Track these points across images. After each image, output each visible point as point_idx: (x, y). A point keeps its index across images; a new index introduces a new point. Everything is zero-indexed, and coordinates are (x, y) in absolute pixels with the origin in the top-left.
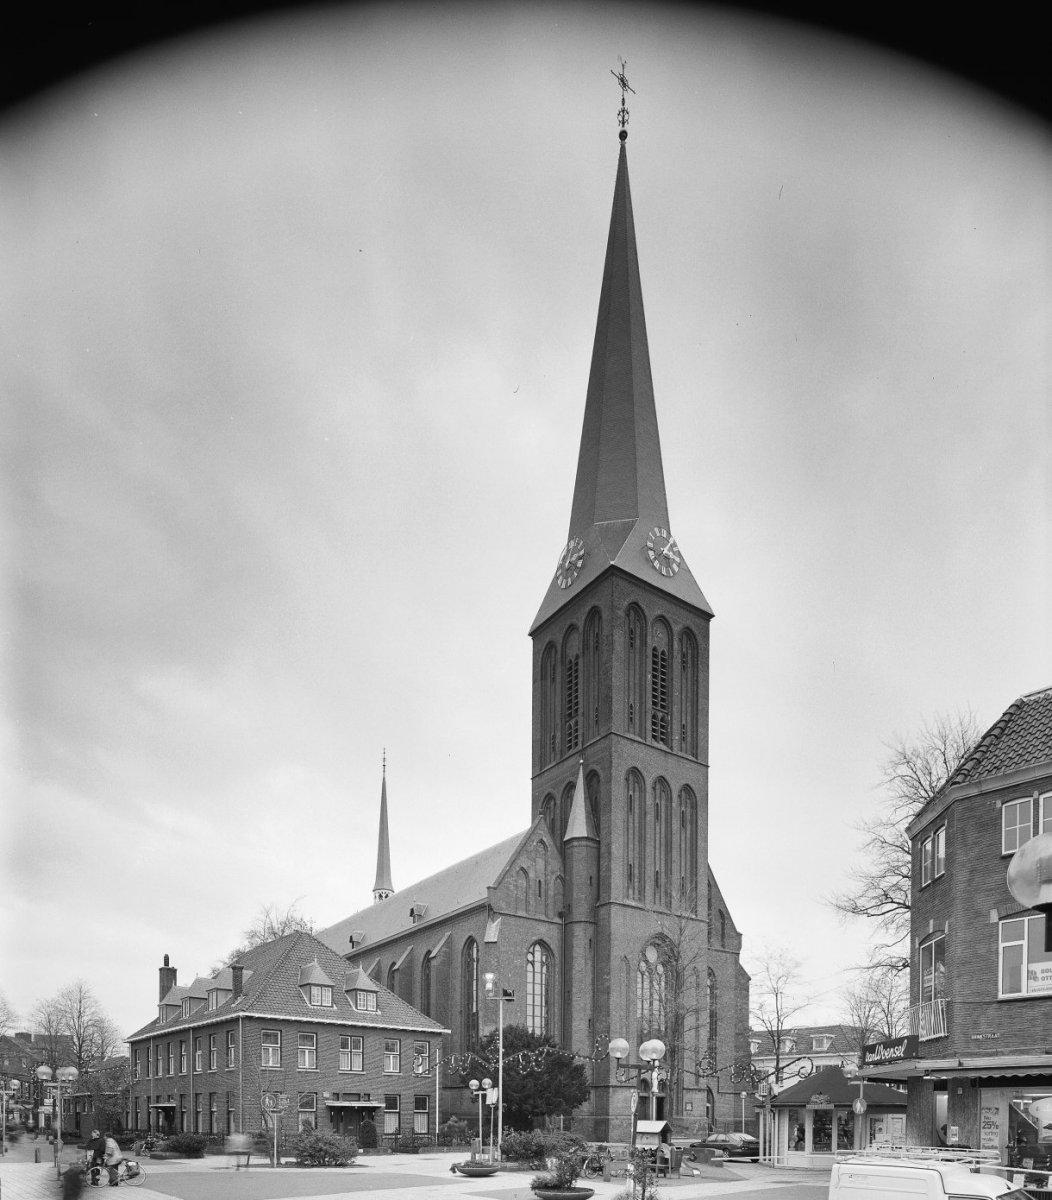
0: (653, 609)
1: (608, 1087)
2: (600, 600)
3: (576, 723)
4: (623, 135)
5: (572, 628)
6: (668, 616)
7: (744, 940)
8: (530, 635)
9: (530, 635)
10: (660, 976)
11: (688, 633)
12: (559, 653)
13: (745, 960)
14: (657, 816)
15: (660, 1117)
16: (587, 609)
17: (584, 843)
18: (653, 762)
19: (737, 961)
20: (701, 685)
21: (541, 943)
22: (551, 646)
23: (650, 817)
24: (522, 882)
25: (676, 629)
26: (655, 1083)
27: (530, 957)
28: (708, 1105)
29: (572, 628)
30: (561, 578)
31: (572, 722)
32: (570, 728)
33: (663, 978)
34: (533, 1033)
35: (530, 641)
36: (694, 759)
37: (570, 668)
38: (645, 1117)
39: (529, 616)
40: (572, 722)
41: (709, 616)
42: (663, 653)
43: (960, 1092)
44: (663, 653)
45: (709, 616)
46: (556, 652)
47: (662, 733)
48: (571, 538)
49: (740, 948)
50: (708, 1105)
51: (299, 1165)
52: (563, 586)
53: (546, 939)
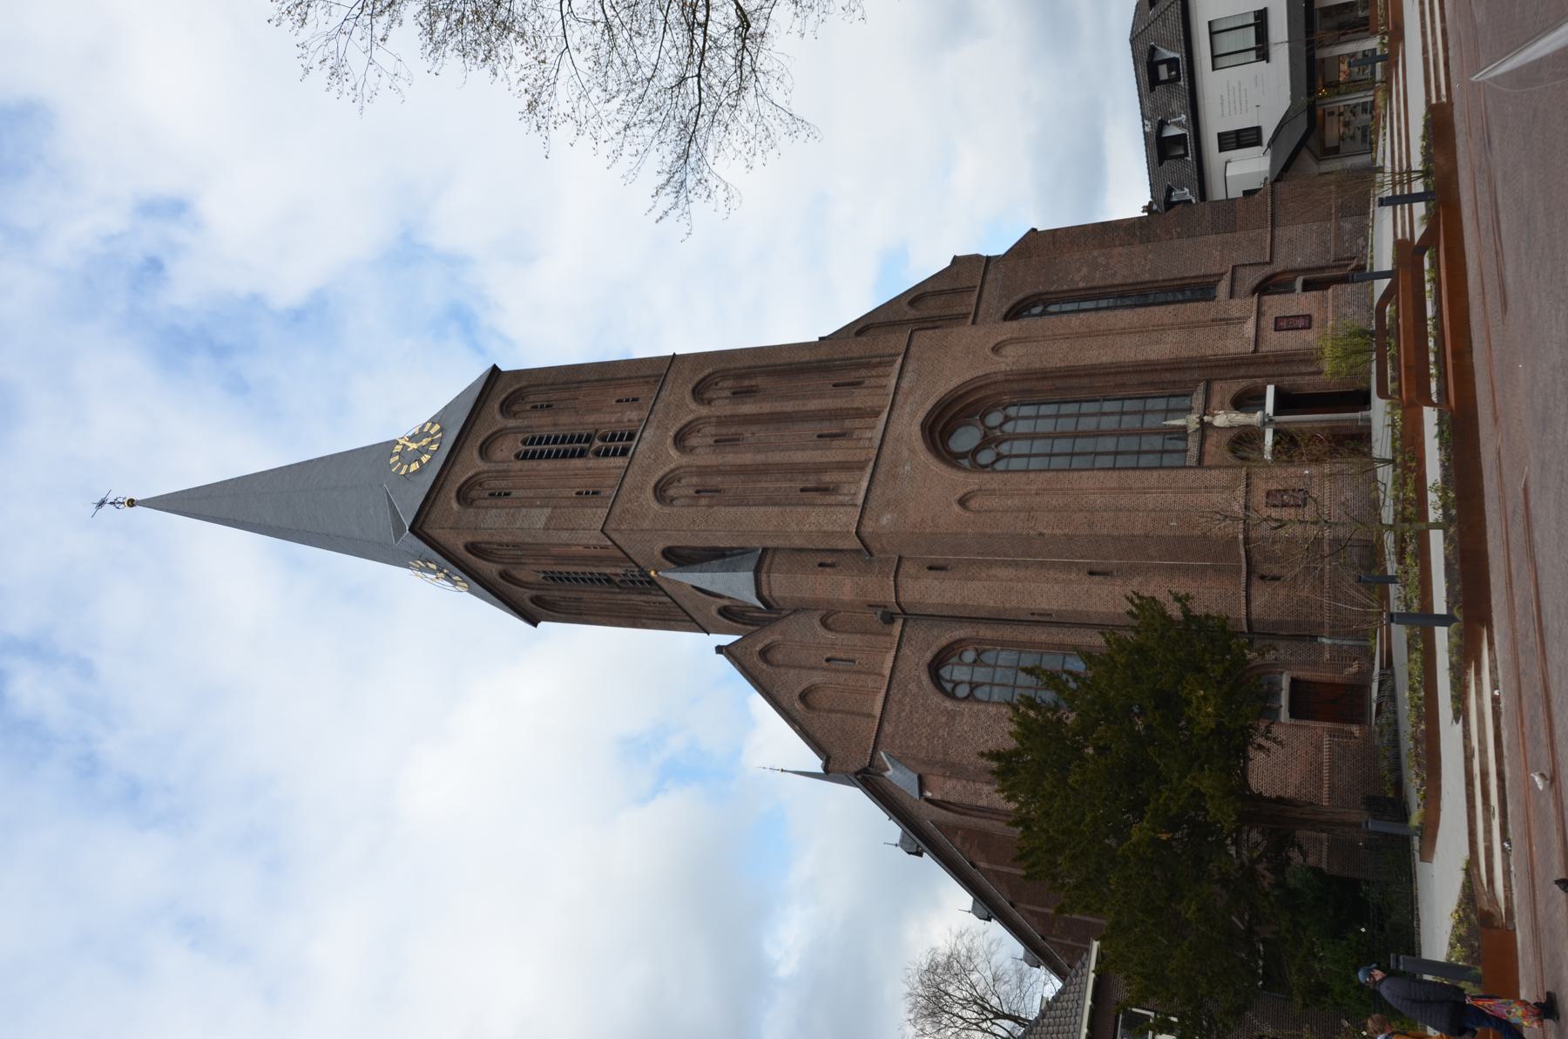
2: (457, 543)
4: (131, 503)
5: (505, 575)
7: (963, 252)
10: (1007, 419)
11: (506, 408)
15: (1362, 401)
17: (764, 577)
21: (935, 668)
25: (501, 422)
26: (1240, 418)
27: (962, 691)
28: (1299, 284)
32: (622, 581)
33: (1012, 411)
34: (1088, 656)
35: (542, 625)
36: (899, 360)
38: (1362, 437)
42: (524, 443)
49: (978, 257)
50: (1299, 284)
53: (929, 656)
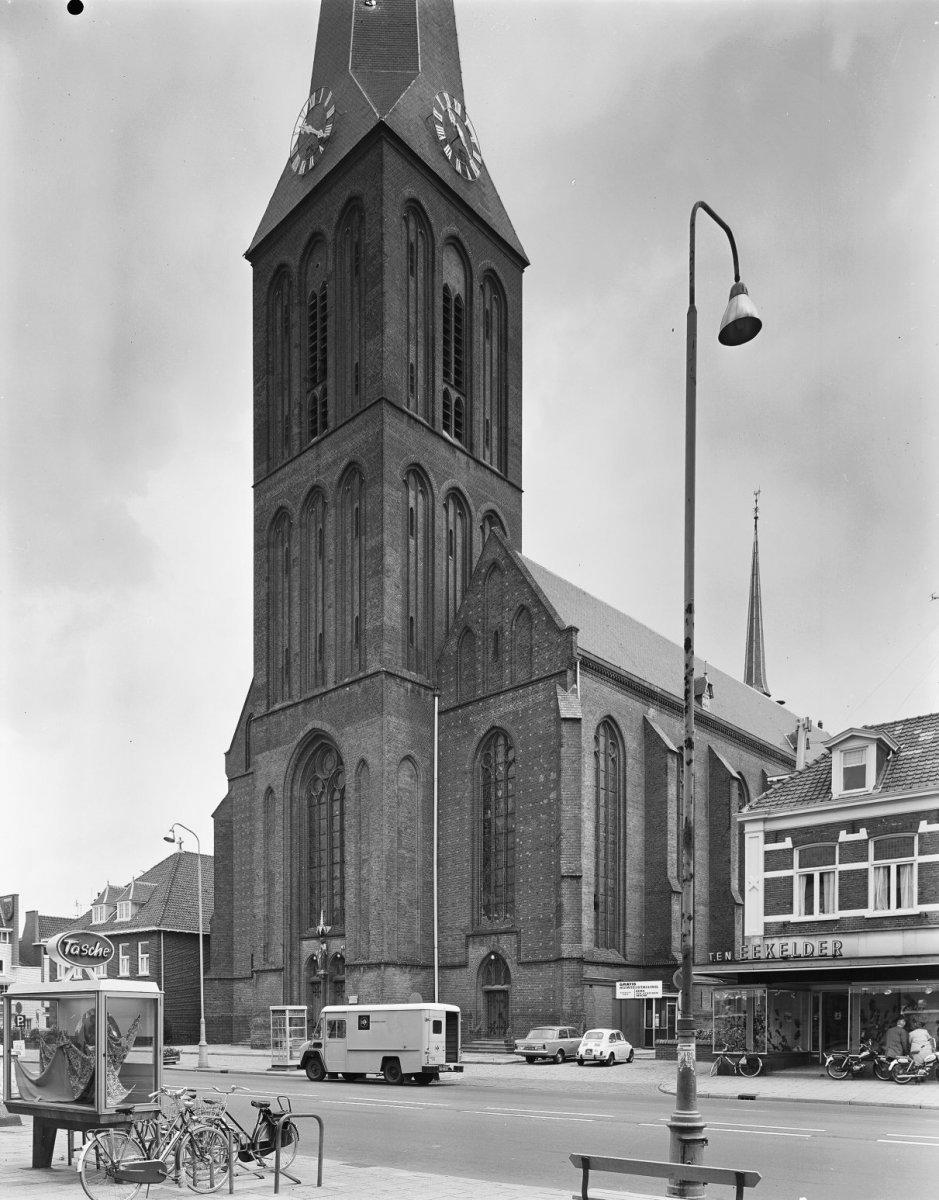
0: (445, 224)
1: (810, 990)
3: (325, 393)
5: (316, 239)
6: (462, 236)
8: (249, 256)
9: (249, 256)
12: (296, 283)
13: (220, 788)
14: (451, 551)
16: (340, 204)
18: (453, 470)
19: (230, 791)
20: (511, 376)
22: (282, 271)
23: (441, 547)
24: (415, 500)
29: (316, 239)
30: (298, 158)
31: (318, 391)
35: (247, 268)
37: (314, 306)
39: (247, 225)
40: (318, 391)
41: (526, 263)
43: (493, 957)
44: (458, 298)
45: (526, 263)
46: (290, 284)
47: (458, 419)
48: (315, 88)
51: (365, 1074)
52: (302, 171)
